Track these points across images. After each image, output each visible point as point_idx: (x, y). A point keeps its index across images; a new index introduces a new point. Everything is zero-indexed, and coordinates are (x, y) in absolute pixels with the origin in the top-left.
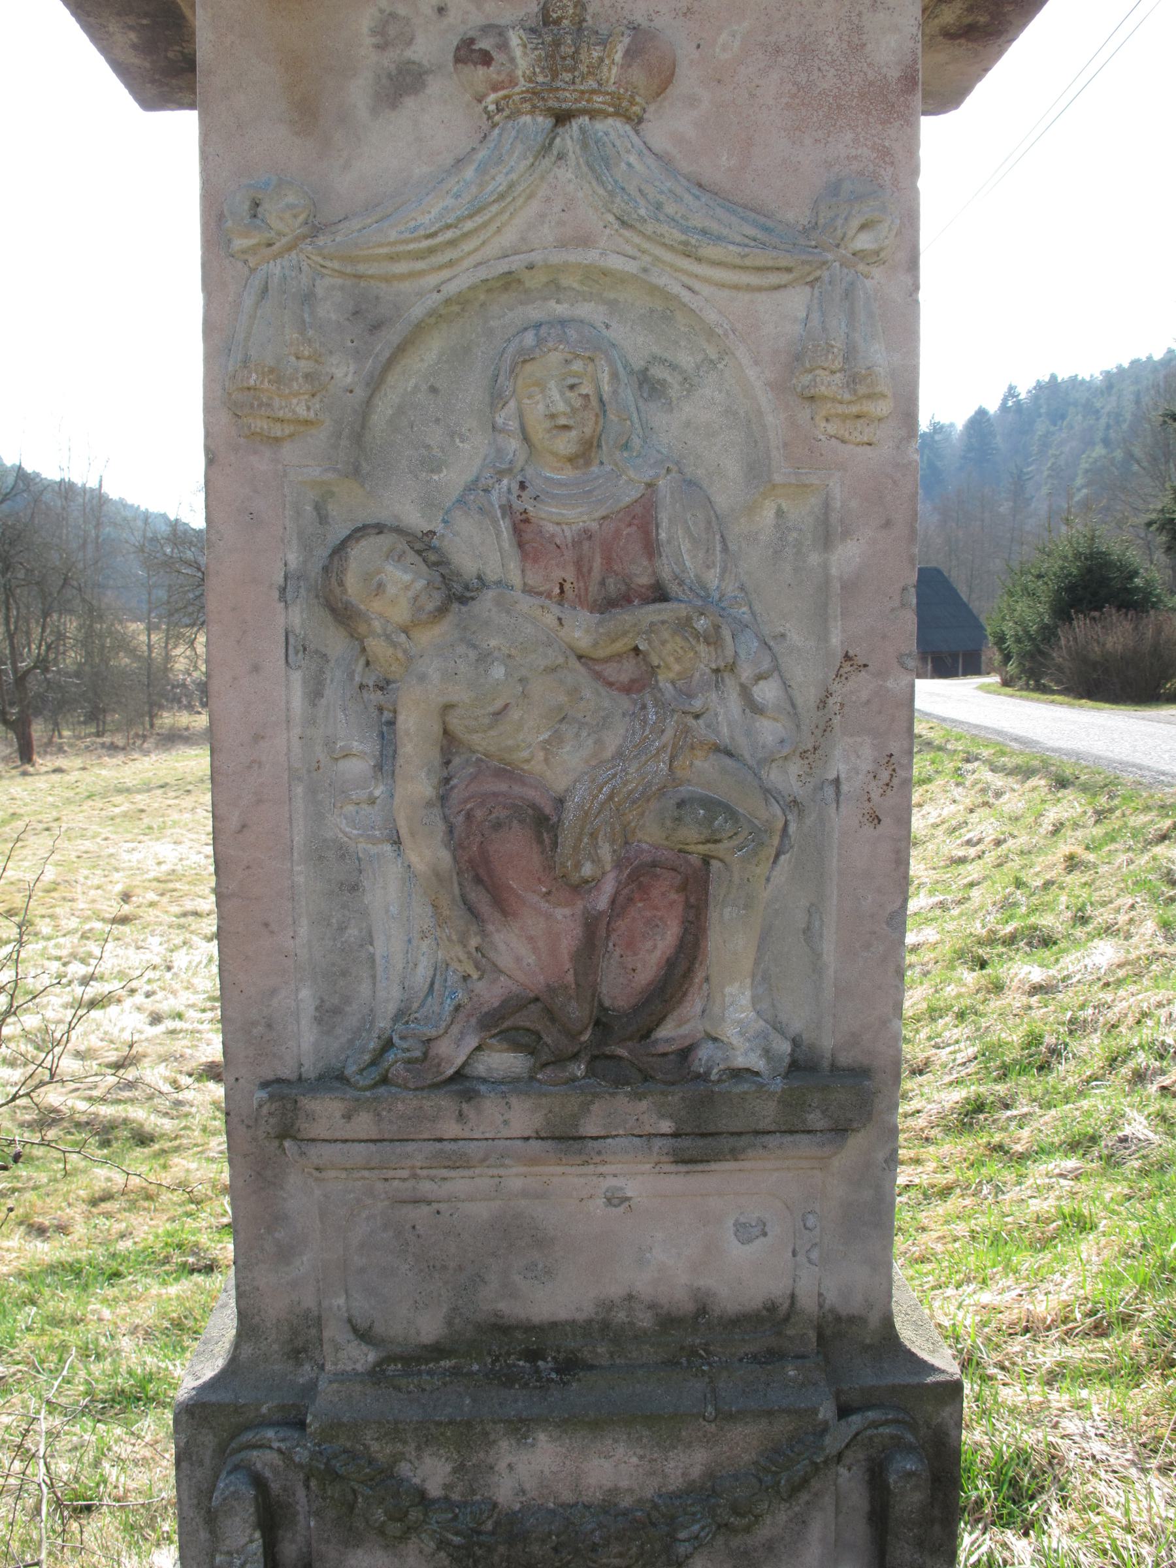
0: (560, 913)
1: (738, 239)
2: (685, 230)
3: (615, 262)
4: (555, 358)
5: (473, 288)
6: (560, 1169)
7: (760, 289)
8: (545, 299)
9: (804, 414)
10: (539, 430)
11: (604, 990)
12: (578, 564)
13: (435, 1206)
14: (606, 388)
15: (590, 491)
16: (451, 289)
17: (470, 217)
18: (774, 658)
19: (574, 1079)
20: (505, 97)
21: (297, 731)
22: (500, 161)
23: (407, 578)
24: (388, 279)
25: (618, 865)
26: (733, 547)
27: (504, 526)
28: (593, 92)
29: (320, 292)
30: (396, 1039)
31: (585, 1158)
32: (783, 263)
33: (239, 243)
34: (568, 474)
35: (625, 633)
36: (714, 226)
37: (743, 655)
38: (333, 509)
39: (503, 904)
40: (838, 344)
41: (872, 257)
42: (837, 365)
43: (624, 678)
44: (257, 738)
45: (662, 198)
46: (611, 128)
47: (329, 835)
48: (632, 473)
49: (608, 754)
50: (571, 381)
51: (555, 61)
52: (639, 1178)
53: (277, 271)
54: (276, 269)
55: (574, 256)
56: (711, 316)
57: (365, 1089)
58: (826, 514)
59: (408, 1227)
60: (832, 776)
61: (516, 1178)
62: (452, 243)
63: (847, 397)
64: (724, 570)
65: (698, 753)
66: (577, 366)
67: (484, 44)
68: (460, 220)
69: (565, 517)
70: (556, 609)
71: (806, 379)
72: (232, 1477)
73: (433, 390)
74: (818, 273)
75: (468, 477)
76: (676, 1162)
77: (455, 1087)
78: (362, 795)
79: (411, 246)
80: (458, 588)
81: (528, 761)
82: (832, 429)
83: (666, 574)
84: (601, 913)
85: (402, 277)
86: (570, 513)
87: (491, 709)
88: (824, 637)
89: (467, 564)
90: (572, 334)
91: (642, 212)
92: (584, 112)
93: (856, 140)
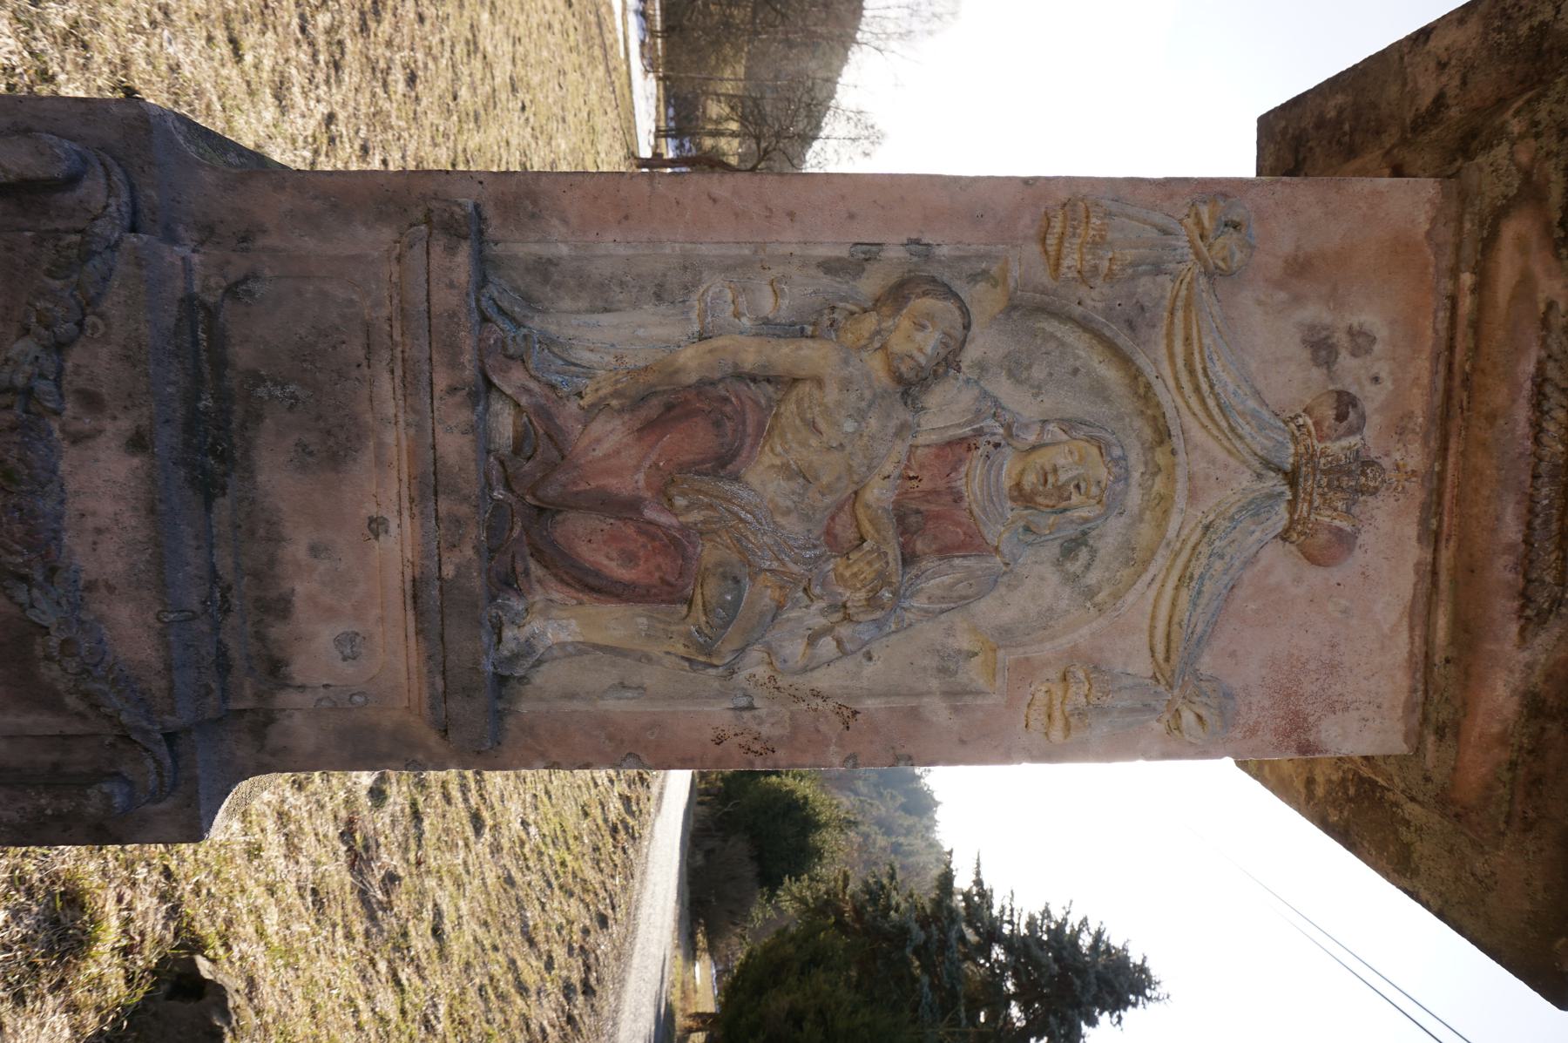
0: (641, 477)
1: (1193, 620)
2: (1202, 577)
3: (1174, 522)
4: (1103, 473)
5: (1158, 405)
6: (405, 477)
7: (1152, 636)
8: (1146, 464)
9: (1054, 674)
10: (1042, 459)
11: (572, 515)
12: (935, 492)
13: (365, 363)
14: (1076, 514)
15: (992, 501)
16: (1158, 387)
17: (1219, 405)
18: (853, 652)
19: (492, 489)
20: (1310, 434)
21: (797, 250)
22: (1261, 428)
23: (929, 350)
24: (1170, 336)
25: (684, 528)
26: (943, 617)
27: (967, 430)
28: (1311, 503)
29: (1160, 279)
30: (524, 331)
31: (417, 499)
32: (1173, 657)
33: (1205, 212)
34: (1007, 483)
35: (878, 531)
36: (1203, 601)
37: (860, 627)
38: (982, 286)
39: (649, 429)
40: (1108, 701)
41: (1175, 727)
42: (1093, 700)
43: (838, 529)
44: (791, 215)
45: (1227, 558)
46: (1280, 517)
47: (705, 275)
48: (1005, 535)
49: (779, 519)
50: (1083, 485)
51: (1336, 471)
52: (398, 547)
53: (1180, 243)
54: (1182, 243)
55: (1181, 486)
56: (1130, 598)
57: (478, 300)
58: (971, 693)
59: (344, 337)
60: (757, 703)
61: (395, 439)
62: (1197, 389)
63: (1068, 708)
64: (926, 611)
65: (777, 594)
66: (1094, 490)
67: (1352, 416)
68: (1217, 396)
69: (973, 480)
70: (897, 472)
71: (1081, 675)
72: (75, 157)
73: (1075, 371)
74: (1163, 682)
75: (1004, 401)
76: (414, 580)
77: (481, 383)
78: (743, 307)
79: (1197, 356)
80: (914, 391)
81: (772, 450)
82: (1041, 696)
83: (924, 564)
84: (641, 514)
85: (1170, 347)
86: (976, 485)
87: (818, 420)
88: (872, 694)
89: (935, 398)
90: (1119, 487)
91: (1217, 543)
92: (1295, 496)
93: (1263, 708)
